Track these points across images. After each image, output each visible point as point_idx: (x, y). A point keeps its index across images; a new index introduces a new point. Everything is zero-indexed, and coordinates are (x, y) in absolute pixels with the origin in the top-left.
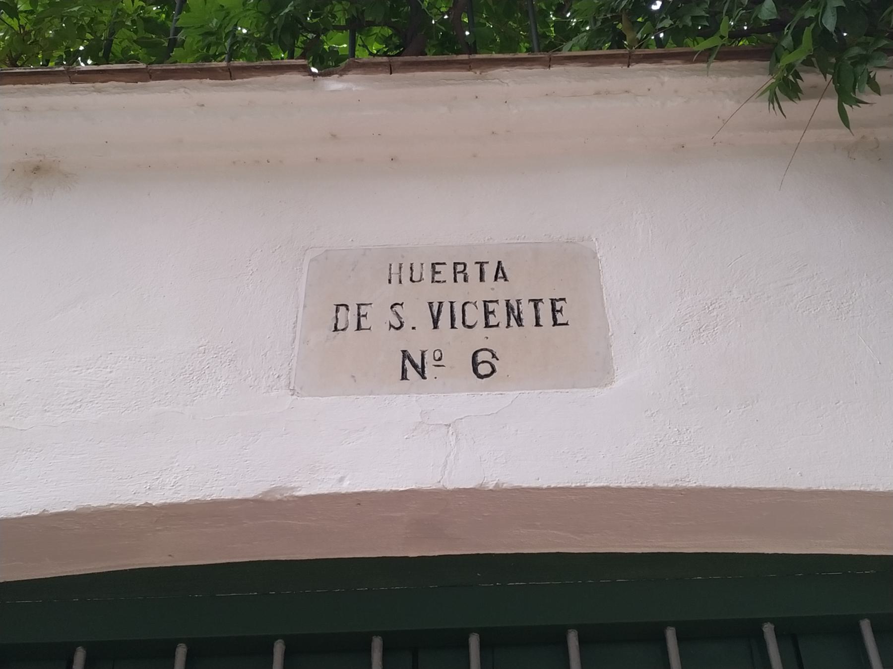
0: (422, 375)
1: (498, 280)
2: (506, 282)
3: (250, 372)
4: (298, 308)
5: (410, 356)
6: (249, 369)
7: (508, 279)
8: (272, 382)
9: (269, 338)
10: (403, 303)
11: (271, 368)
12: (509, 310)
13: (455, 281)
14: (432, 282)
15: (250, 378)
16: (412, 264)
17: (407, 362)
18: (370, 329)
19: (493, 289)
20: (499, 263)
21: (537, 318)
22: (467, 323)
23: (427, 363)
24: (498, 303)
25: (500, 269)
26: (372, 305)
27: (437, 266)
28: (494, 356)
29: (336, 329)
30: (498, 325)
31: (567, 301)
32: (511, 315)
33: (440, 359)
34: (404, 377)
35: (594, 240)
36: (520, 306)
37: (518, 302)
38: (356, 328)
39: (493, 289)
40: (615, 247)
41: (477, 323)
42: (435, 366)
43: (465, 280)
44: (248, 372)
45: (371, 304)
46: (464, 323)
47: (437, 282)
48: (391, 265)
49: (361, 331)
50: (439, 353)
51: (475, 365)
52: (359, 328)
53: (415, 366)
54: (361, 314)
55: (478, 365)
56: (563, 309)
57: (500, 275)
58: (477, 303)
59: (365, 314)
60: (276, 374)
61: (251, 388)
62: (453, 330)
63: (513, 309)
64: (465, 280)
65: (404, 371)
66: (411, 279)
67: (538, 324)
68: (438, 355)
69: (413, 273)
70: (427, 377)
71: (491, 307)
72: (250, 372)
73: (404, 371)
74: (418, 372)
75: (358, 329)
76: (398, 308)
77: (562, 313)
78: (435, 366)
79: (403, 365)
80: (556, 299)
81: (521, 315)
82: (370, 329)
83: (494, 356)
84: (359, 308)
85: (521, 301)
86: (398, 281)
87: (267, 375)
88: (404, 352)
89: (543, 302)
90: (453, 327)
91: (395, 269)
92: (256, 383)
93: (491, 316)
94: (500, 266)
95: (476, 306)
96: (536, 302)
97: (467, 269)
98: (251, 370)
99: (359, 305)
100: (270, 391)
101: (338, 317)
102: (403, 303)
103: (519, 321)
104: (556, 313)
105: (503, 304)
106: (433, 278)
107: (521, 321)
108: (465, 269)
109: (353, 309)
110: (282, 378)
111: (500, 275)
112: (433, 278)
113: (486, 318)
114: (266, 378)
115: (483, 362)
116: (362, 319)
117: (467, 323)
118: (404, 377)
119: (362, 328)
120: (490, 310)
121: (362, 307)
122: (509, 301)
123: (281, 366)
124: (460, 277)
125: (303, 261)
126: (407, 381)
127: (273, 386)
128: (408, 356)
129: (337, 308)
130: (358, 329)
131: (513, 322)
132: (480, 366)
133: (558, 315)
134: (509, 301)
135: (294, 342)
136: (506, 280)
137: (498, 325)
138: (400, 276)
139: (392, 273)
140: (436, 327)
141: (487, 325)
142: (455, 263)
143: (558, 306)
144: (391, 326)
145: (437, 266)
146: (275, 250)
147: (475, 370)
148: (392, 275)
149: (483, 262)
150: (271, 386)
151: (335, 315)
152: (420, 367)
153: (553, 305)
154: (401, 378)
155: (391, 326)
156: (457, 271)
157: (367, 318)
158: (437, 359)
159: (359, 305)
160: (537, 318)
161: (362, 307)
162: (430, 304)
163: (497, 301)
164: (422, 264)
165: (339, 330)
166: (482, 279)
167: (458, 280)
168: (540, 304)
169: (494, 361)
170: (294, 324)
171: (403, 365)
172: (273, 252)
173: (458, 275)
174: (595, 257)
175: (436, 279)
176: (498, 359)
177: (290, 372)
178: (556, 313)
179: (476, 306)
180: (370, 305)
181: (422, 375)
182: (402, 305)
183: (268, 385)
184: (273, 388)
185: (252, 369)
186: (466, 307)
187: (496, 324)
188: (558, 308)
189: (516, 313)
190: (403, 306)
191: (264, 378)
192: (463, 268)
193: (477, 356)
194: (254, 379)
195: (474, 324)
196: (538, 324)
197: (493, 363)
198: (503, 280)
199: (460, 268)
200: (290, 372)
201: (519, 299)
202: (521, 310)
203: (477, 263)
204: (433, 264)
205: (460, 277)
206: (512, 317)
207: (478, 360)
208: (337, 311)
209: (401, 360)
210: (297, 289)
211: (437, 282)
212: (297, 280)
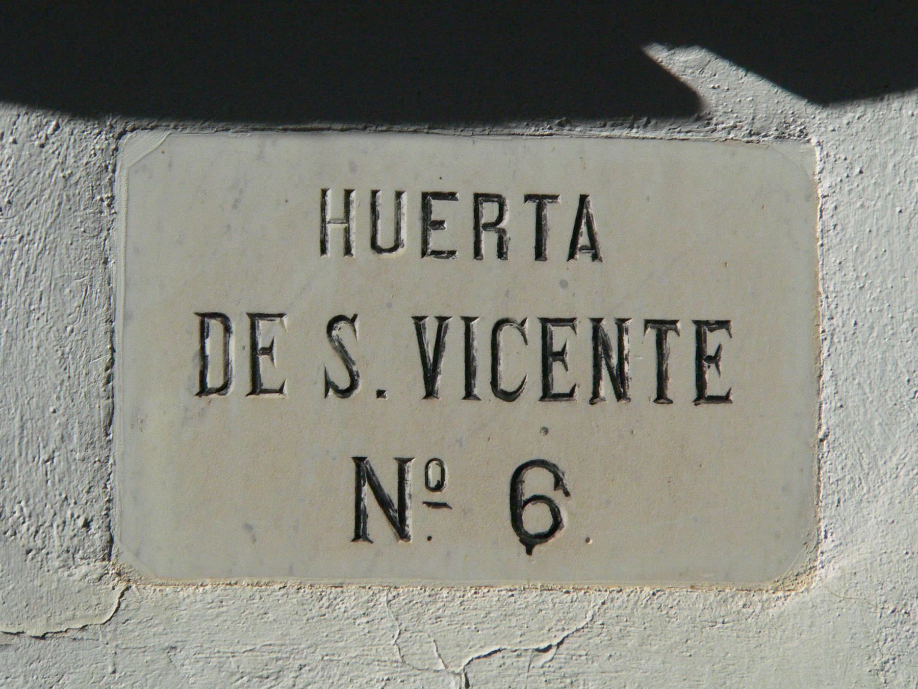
0: (400, 529)
1: (578, 256)
2: (597, 262)
3: (22, 509)
4: (110, 321)
5: (374, 475)
6: (20, 502)
7: (601, 254)
8: (72, 538)
9: (54, 412)
10: (355, 316)
11: (66, 498)
12: (600, 348)
13: (477, 253)
14: (424, 253)
15: (25, 525)
16: (374, 193)
17: (366, 489)
18: (280, 391)
19: (564, 284)
20: (583, 199)
21: (662, 378)
22: (504, 385)
23: (410, 496)
24: (574, 328)
25: (584, 221)
26: (285, 319)
27: (435, 204)
28: (558, 482)
29: (203, 390)
30: (570, 395)
31: (732, 331)
32: (603, 363)
33: (439, 487)
34: (360, 534)
35: (814, 141)
36: (625, 338)
37: (621, 323)
38: (248, 388)
39: (564, 284)
40: (861, 172)
41: (526, 386)
42: (429, 504)
43: (501, 253)
44: (17, 508)
45: (281, 315)
46: (494, 383)
47: (437, 254)
48: (324, 193)
49: (262, 396)
50: (439, 469)
51: (517, 505)
52: (256, 387)
53: (383, 502)
54: (260, 346)
55: (523, 508)
56: (723, 354)
57: (583, 240)
58: (527, 325)
59: (268, 345)
60: (78, 517)
61: (30, 555)
62: (470, 403)
63: (607, 349)
64: (501, 253)
65: (360, 515)
66: (374, 245)
67: (661, 396)
68: (434, 475)
69: (379, 222)
70: (411, 533)
71: (439, 209)
72: (22, 509)
73: (360, 515)
74: (390, 519)
75: (253, 392)
76: (342, 331)
77: (717, 367)
78: (429, 504)
79: (359, 500)
80: (707, 323)
81: (627, 368)
82: (280, 391)
83: (558, 482)
84: (253, 328)
85: (628, 323)
86: (342, 251)
87: (58, 520)
88: (359, 461)
89: (676, 330)
90: (469, 394)
91: (334, 208)
92: (39, 543)
93: (557, 367)
94: (585, 211)
95: (523, 335)
96: (540, 201)
97: (507, 216)
98: (23, 503)
99: (254, 318)
100: (70, 562)
101: (208, 351)
102: (355, 316)
103: (620, 381)
104: (706, 364)
105: (585, 329)
106: (425, 242)
107: (623, 387)
108: (500, 218)
109: (241, 327)
110: (94, 526)
111: (583, 240)
112: (425, 242)
113: (546, 370)
114: (58, 526)
115: (536, 499)
116: (263, 359)
117: (504, 385)
118: (360, 534)
119: (266, 386)
120: (557, 348)
121: (262, 324)
122: (599, 320)
123: (88, 492)
124: (489, 240)
125: (114, 171)
126: (366, 543)
127: (76, 551)
128: (368, 472)
129: (202, 323)
130: (253, 392)
131: (606, 388)
132: (526, 508)
133: (710, 374)
134: (599, 320)
135: (110, 423)
136: (595, 257)
137: (570, 395)
138: (347, 231)
139: (328, 218)
140: (430, 392)
141: (547, 394)
142: (477, 196)
143: (713, 340)
144: (329, 384)
145: (435, 204)
146: (47, 138)
147: (516, 521)
148: (328, 226)
149: (545, 197)
150: (72, 551)
151: (197, 346)
152: (396, 506)
153: (700, 339)
154: (352, 535)
155: (329, 384)
156: (483, 221)
157: (272, 359)
158: (433, 484)
159: (254, 318)
160: (662, 378)
161: (262, 324)
162: (419, 321)
163: (451, 196)
164: (399, 195)
165: (211, 392)
166: (540, 254)
167: (483, 251)
168: (671, 335)
169: (558, 497)
170: (107, 369)
171: (359, 500)
172: (42, 146)
173: (484, 235)
174: (810, 195)
175: (432, 246)
176: (567, 494)
177: (108, 509)
178: (706, 364)
179: (523, 335)
180: (278, 319)
181: (400, 529)
182: (352, 321)
183: (64, 547)
184: (78, 556)
185: (27, 502)
186: (502, 336)
187: (568, 391)
188: (710, 351)
189: (614, 361)
190: (357, 324)
191: (55, 526)
192: (496, 214)
193: (522, 482)
194: (33, 529)
195: (517, 387)
196: (661, 396)
197: (557, 502)
198: (587, 257)
199: (489, 212)
200: (108, 509)
201: (623, 317)
202: (626, 352)
203: (528, 198)
204: (425, 195)
205: (489, 240)
206: (605, 372)
207: (523, 494)
208: (204, 333)
209: (352, 490)
210: (106, 262)
211: (437, 254)
212: (105, 233)
